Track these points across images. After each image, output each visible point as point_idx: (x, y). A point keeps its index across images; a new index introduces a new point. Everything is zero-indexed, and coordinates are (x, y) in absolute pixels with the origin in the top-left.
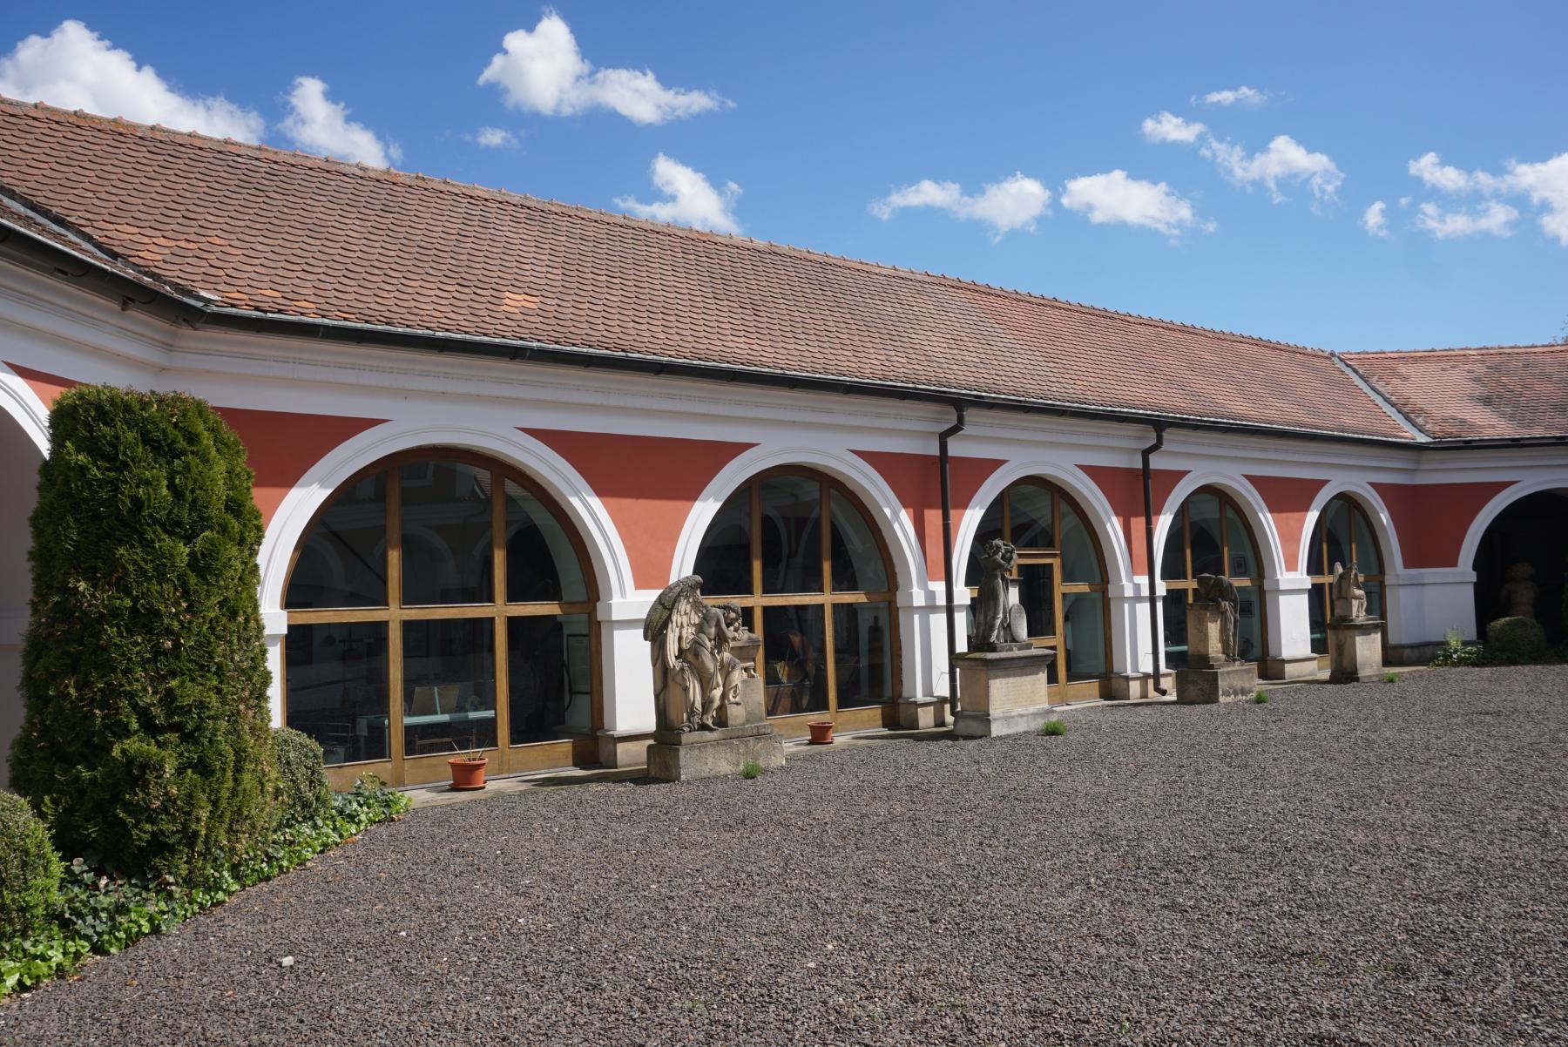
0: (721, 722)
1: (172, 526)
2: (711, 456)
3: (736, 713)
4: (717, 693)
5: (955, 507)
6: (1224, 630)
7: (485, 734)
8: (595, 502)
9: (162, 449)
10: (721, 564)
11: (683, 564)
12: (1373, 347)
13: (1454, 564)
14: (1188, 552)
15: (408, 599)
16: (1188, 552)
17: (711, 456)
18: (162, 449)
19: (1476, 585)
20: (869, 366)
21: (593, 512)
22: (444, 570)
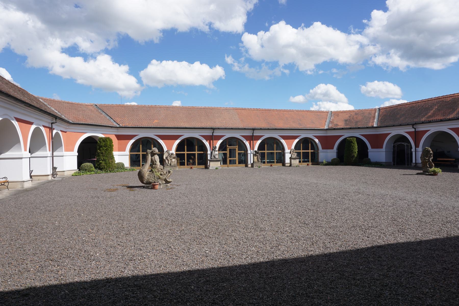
0: (170, 165)
1: (105, 147)
2: (261, 137)
3: (172, 164)
4: (170, 162)
5: (255, 140)
6: (257, 158)
7: (273, 162)
8: (283, 140)
9: (104, 141)
10: (297, 147)
11: (293, 147)
12: (361, 108)
13: (73, 151)
14: (186, 147)
15: (187, 151)
16: (186, 147)
17: (261, 137)
18: (104, 141)
19: (78, 156)
20: (203, 125)
21: (283, 141)
22: (191, 148)
